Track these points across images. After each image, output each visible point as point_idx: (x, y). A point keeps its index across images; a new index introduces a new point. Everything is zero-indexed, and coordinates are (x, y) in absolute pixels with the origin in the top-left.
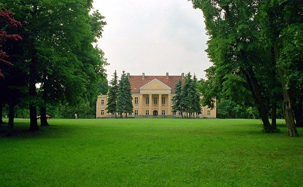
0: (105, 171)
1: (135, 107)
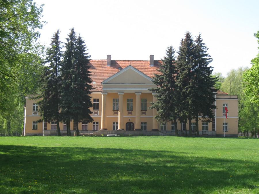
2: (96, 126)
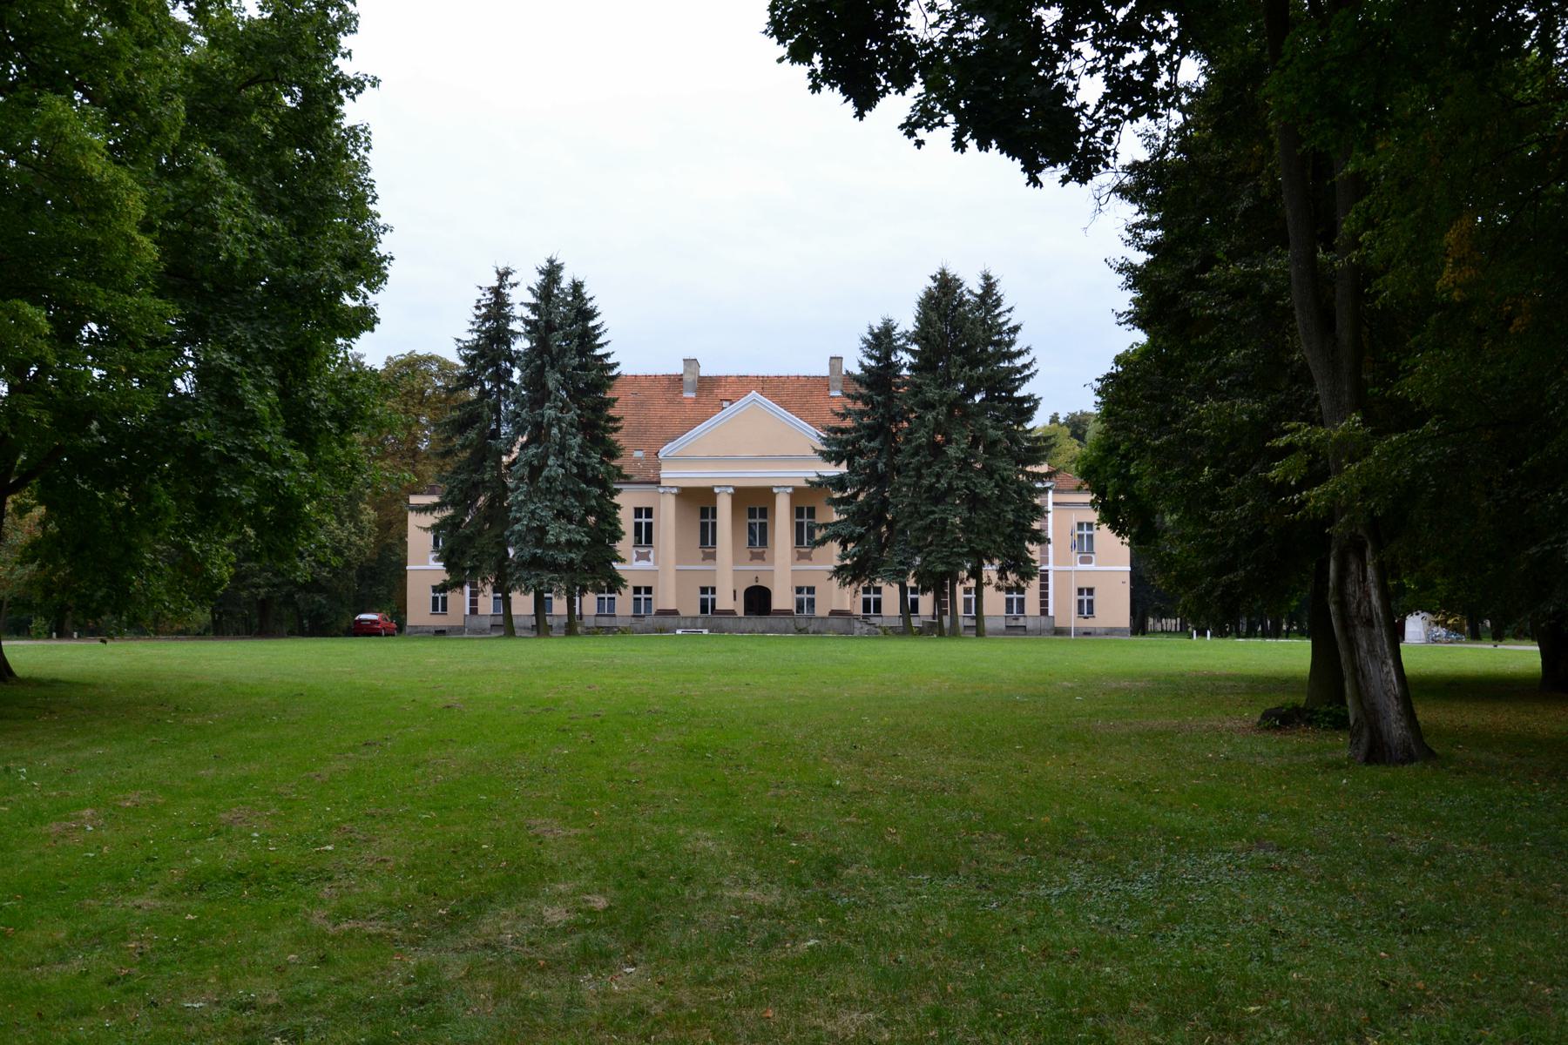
0: (1440, 861)
1: (631, 565)
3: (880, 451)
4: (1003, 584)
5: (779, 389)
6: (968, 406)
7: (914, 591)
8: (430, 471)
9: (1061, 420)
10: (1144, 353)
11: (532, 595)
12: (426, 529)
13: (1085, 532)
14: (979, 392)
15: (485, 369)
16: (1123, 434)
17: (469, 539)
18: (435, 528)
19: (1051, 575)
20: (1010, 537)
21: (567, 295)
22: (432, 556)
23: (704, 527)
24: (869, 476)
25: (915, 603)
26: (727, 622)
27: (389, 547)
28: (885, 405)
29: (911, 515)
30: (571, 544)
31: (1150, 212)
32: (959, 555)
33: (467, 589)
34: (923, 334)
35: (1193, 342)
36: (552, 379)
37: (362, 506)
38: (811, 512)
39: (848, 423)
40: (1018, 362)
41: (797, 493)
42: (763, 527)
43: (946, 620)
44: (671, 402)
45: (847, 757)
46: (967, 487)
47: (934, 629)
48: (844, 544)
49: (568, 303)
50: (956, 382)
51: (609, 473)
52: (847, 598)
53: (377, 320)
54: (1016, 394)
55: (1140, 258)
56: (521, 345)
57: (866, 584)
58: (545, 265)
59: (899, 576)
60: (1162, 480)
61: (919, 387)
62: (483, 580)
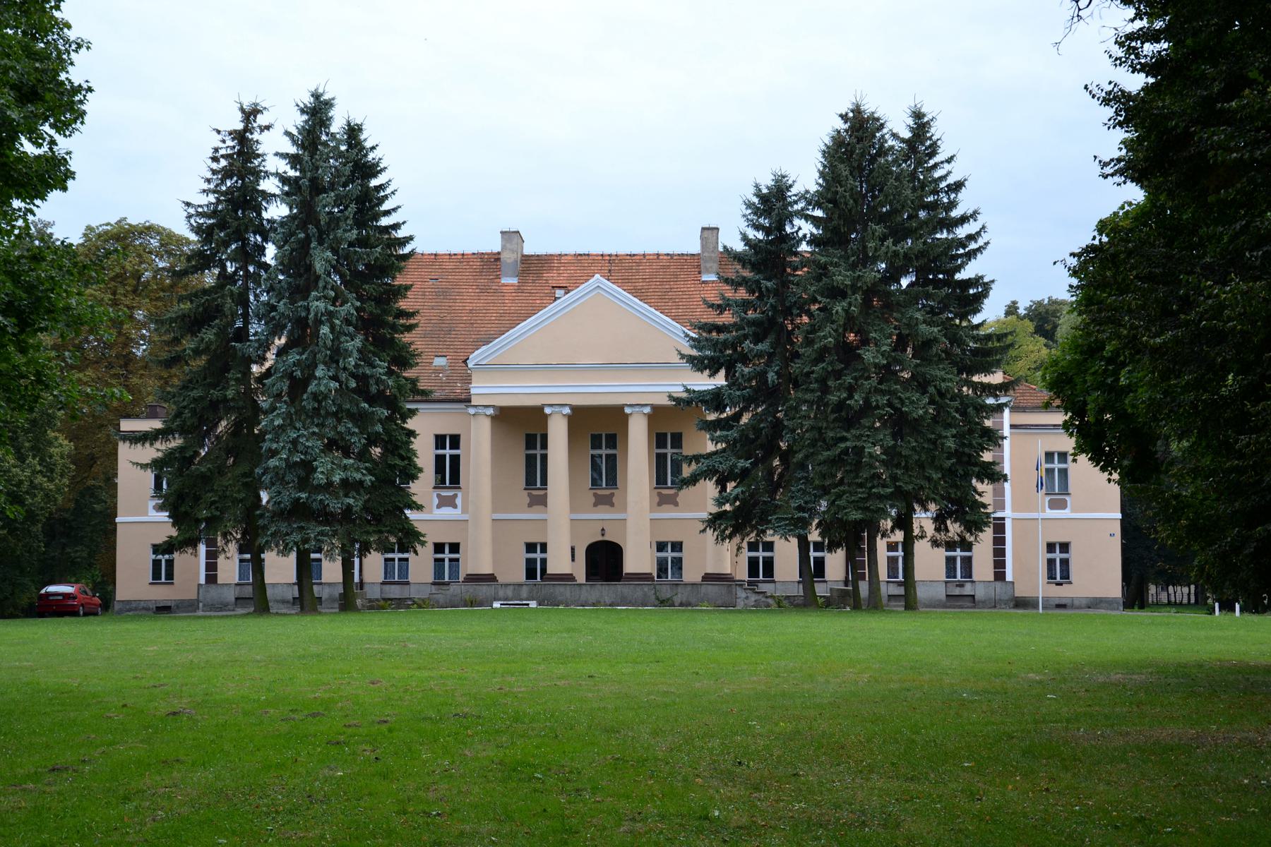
1: (431, 513)
2: (451, 560)
3: (771, 355)
4: (941, 537)
5: (629, 271)
6: (890, 293)
7: (818, 547)
8: (152, 385)
9: (1022, 311)
10: (1140, 216)
11: (293, 556)
12: (144, 466)
13: (1057, 465)
14: (906, 273)
15: (227, 245)
16: (1109, 329)
17: (205, 479)
18: (157, 465)
19: (1008, 524)
20: (951, 472)
21: (339, 142)
22: (152, 503)
23: (530, 461)
24: (757, 390)
25: (820, 563)
26: (562, 591)
27: (91, 491)
28: (776, 293)
29: (813, 444)
30: (348, 486)
31: (1152, 17)
32: (881, 497)
33: (202, 548)
34: (829, 195)
35: (1211, 199)
36: (321, 259)
37: (51, 434)
38: (677, 440)
39: (727, 318)
40: (962, 232)
41: (657, 415)
42: (612, 460)
43: (864, 587)
44: (484, 290)
45: (729, 777)
46: (890, 405)
47: (847, 599)
48: (722, 483)
49: (341, 155)
50: (875, 259)
51: (400, 388)
52: (727, 557)
53: (70, 175)
54: (958, 276)
55: (1135, 82)
56: (277, 211)
57: (752, 537)
58: (308, 100)
59: (797, 526)
60: (1166, 393)
61: (824, 267)
62: (224, 535)
